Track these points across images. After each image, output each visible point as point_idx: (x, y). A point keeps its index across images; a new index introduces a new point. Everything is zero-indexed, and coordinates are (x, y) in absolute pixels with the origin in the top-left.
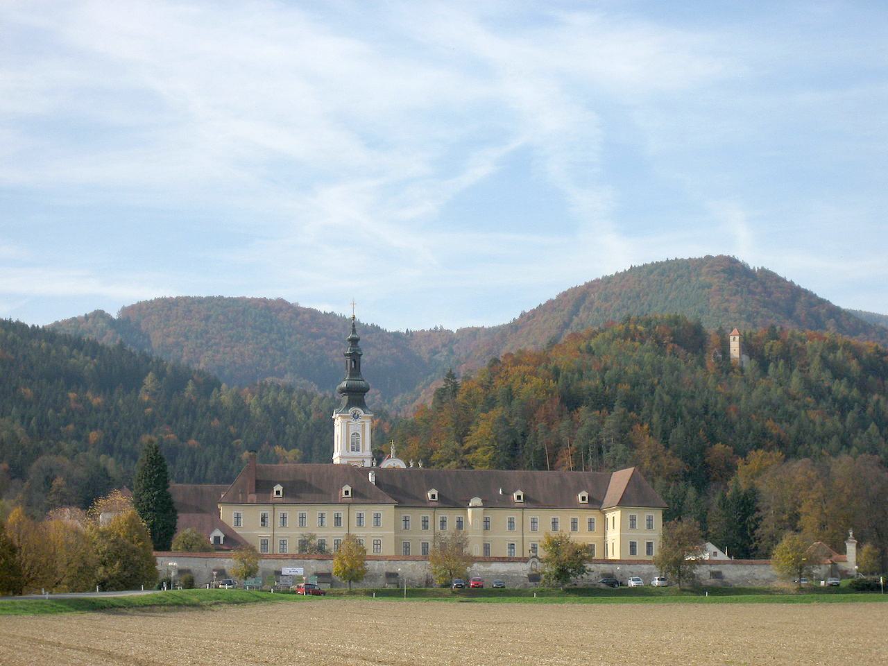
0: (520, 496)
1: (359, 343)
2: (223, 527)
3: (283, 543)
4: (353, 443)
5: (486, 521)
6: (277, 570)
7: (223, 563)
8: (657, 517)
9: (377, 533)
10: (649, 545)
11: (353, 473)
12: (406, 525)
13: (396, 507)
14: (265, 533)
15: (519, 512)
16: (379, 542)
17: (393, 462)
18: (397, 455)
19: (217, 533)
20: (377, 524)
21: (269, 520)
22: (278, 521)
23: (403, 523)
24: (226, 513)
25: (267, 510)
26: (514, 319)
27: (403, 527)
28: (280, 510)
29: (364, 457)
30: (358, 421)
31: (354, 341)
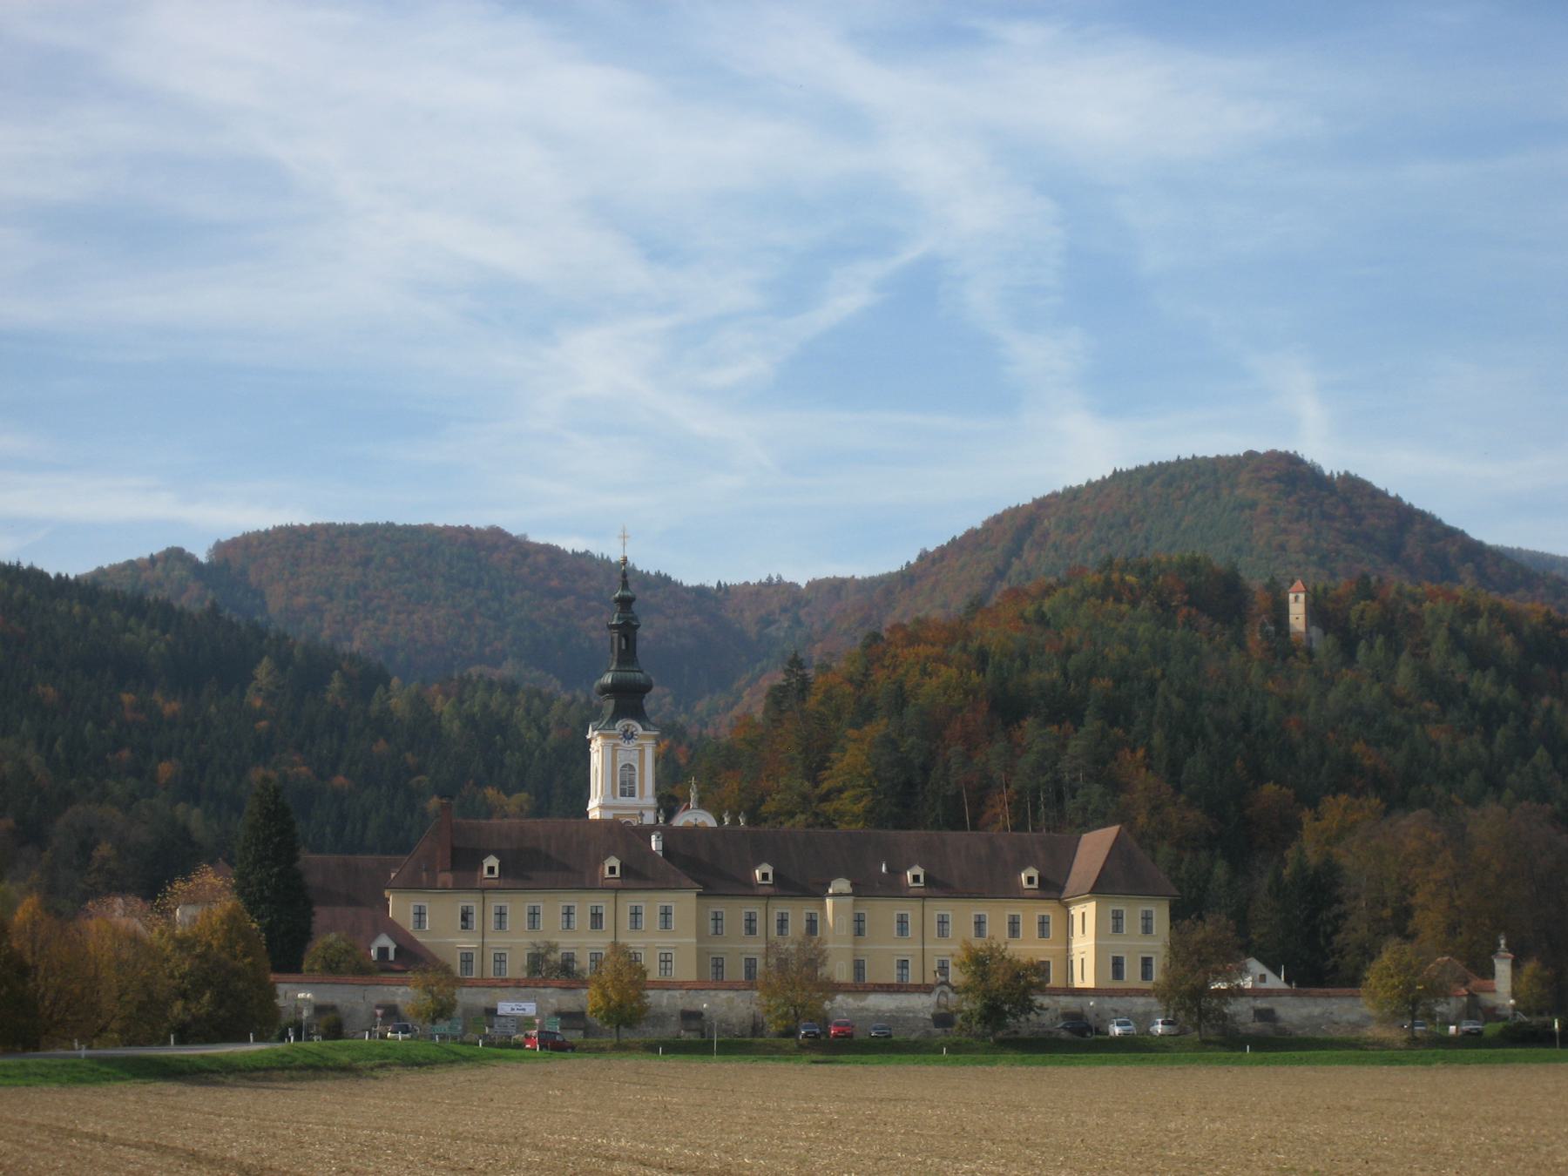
2: (394, 930)
4: (623, 783)
5: (859, 920)
8: (1161, 913)
9: (665, 941)
10: (1147, 962)
11: (624, 836)
14: (468, 942)
17: (693, 817)
18: (702, 804)
19: (384, 941)
22: (492, 918)
24: (399, 907)
30: (633, 743)
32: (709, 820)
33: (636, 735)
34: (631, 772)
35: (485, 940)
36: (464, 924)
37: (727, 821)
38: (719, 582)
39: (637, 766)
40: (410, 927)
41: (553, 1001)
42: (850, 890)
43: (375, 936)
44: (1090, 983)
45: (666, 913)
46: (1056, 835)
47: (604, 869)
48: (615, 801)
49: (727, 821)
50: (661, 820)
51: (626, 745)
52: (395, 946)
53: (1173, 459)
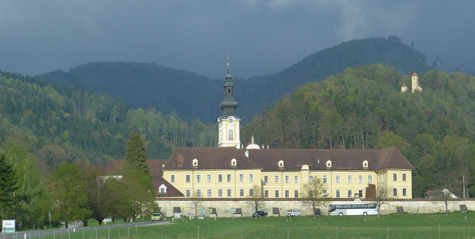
3: (287, 192)
4: (230, 136)
6: (276, 207)
7: (179, 203)
8: (409, 174)
9: (209, 186)
10: (404, 190)
11: (231, 151)
13: (262, 170)
14: (189, 186)
15: (329, 173)
16: (210, 191)
17: (253, 146)
18: (256, 142)
19: (163, 186)
20: (228, 180)
22: (196, 179)
24: (167, 175)
28: (197, 173)
29: (236, 143)
32: (257, 147)
33: (233, 121)
34: (232, 133)
35: (235, 185)
37: (263, 147)
38: (342, 41)
39: (234, 131)
41: (231, 205)
42: (308, 168)
43: (160, 185)
44: (161, 192)
45: (229, 176)
46: (372, 150)
47: (231, 163)
48: (227, 142)
49: (263, 147)
50: (242, 147)
51: (230, 124)
52: (167, 188)
53: (332, 46)
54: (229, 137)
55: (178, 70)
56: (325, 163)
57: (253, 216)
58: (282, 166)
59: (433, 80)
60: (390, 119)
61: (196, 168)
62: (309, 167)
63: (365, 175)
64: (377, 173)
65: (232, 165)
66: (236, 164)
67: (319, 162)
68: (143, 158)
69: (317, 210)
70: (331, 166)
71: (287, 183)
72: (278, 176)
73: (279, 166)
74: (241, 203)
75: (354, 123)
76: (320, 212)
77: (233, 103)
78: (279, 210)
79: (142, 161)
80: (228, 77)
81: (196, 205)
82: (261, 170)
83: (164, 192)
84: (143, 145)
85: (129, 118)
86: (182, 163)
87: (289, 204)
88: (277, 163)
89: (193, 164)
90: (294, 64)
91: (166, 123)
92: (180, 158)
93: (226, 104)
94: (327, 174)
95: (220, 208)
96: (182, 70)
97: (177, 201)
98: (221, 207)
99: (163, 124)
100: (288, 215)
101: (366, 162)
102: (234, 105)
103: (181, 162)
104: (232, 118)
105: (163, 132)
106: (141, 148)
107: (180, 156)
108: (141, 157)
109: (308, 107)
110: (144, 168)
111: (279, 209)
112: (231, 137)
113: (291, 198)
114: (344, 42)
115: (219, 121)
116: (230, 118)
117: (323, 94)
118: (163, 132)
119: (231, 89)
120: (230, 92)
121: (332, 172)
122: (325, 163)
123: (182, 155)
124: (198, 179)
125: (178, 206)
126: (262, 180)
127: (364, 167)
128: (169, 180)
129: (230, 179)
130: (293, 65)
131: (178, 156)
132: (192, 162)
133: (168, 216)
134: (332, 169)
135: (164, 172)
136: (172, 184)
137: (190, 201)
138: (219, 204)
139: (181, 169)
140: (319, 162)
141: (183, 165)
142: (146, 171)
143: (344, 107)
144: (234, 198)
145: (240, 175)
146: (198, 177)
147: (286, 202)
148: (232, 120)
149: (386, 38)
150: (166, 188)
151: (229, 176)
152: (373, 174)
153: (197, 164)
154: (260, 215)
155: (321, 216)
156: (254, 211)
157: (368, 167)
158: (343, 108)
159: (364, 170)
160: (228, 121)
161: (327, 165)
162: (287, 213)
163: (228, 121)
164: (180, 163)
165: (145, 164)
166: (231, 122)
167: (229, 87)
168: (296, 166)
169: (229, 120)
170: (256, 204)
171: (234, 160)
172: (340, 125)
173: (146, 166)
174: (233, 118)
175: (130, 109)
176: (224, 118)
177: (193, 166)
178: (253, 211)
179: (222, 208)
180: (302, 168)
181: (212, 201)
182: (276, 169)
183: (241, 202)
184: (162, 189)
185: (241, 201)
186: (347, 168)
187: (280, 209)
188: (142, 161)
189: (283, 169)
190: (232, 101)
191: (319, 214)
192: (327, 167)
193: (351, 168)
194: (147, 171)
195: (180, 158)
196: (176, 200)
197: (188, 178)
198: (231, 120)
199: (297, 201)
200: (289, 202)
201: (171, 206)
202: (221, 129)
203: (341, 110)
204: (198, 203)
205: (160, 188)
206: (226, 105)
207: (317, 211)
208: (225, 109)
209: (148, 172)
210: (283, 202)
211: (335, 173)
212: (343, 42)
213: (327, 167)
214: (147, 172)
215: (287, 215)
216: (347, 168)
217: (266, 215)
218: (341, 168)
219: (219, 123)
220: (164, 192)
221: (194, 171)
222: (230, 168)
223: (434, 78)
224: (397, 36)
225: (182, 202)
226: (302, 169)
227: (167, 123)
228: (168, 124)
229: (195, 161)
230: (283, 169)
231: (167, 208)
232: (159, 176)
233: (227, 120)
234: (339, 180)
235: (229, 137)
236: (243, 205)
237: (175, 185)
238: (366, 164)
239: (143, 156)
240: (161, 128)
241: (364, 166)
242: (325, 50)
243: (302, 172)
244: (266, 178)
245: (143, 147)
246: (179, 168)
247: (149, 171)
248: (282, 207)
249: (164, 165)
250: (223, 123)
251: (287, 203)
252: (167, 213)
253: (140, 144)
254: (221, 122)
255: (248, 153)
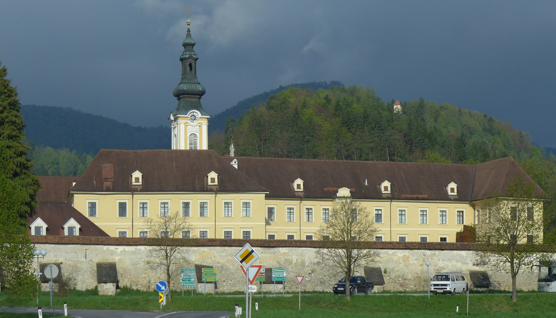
0: (387, 187)
1: (195, 48)
2: (79, 218)
4: (191, 140)
5: (271, 211)
7: (113, 253)
12: (308, 217)
19: (72, 223)
20: (202, 214)
21: (209, 211)
22: (138, 211)
23: (420, 218)
25: (125, 198)
26: (215, 115)
27: (440, 222)
28: (140, 198)
30: (196, 122)
31: (188, 46)
33: (198, 118)
36: (532, 156)
38: (280, 86)
39: (198, 135)
40: (86, 214)
42: (349, 195)
43: (66, 221)
45: (203, 206)
51: (192, 123)
52: (80, 226)
54: (190, 146)
55: (96, 116)
56: (378, 186)
57: (336, 292)
58: (300, 189)
59: (419, 111)
60: (419, 138)
61: (139, 190)
62: (351, 192)
63: (452, 209)
64: (473, 206)
65: (210, 183)
66: (216, 183)
67: (366, 184)
68: (14, 130)
69: (482, 276)
70: (390, 192)
71: (308, 221)
72: (293, 209)
73: (295, 190)
74: (282, 254)
75: (374, 138)
76: (489, 281)
77: (197, 87)
78: (383, 273)
79: (10, 137)
80: (188, 42)
81: (167, 255)
82: (264, 195)
83: (74, 235)
84: (13, 94)
85: (36, 157)
86: (111, 178)
87: (406, 259)
88: (291, 184)
89: (133, 180)
90: (227, 109)
91: (81, 164)
92: (108, 169)
93: (185, 89)
94: (384, 206)
95: (225, 268)
96: (101, 116)
97: (105, 247)
98: (228, 265)
99: (78, 165)
100: (439, 291)
101: (453, 185)
102: (199, 90)
103: (110, 177)
104: (195, 113)
105: (79, 174)
106: (9, 101)
107: (108, 165)
108: (7, 125)
109: (298, 117)
110: (15, 155)
111: (383, 270)
112: (193, 146)
113: (414, 241)
114: (283, 86)
115: (172, 118)
116: (192, 113)
117: (316, 101)
118: (79, 174)
119: (193, 64)
120: (191, 69)
121: (392, 203)
122: (378, 186)
123: (112, 164)
124: (141, 211)
125: (111, 261)
126: (265, 218)
127: (450, 195)
128: (85, 212)
129: (205, 211)
130: (226, 109)
131: (104, 165)
132: (130, 177)
133: (81, 287)
134: (392, 198)
135: (75, 195)
136: (92, 219)
137: (142, 248)
138: (223, 254)
139: (108, 190)
140: (366, 184)
141: (113, 183)
142: (20, 163)
143: (349, 119)
144: (261, 241)
145: (225, 203)
146: (141, 206)
147: (400, 253)
148: (195, 116)
149: (328, 83)
150: (78, 226)
151: (203, 206)
152: (466, 208)
153: (140, 180)
154: (356, 290)
155: (493, 292)
156: (342, 276)
157: (456, 194)
158: (348, 121)
159: (450, 200)
160: (189, 119)
161: (383, 189)
162: (435, 285)
163: (189, 119)
164: (107, 179)
165: (19, 145)
166: (194, 121)
167: (190, 60)
168: (325, 189)
169: (189, 116)
170: (349, 257)
171: (213, 175)
172: (352, 142)
173: (21, 149)
174: (198, 114)
175: (37, 147)
176: (182, 113)
177: (133, 184)
178: (313, 275)
179: (231, 267)
180: (337, 194)
181: (202, 249)
182: (290, 195)
183: (282, 252)
184: (71, 229)
185: (281, 249)
186: (420, 196)
187: (385, 272)
188: (10, 137)
189: (302, 194)
190: (194, 85)
191: (488, 285)
192: (383, 192)
193: (426, 196)
194: (24, 164)
195: (108, 169)
196: (105, 245)
197: (122, 208)
198: (193, 118)
199: (430, 249)
200: (407, 252)
201: (88, 259)
202: (176, 133)
203: (346, 123)
204: (360, 204)
205: (66, 227)
206: (185, 90)
207: (482, 277)
208: (184, 97)
209: (27, 168)
210: (391, 252)
211: (398, 205)
212: (281, 86)
213: (383, 192)
214: (24, 167)
215: (433, 289)
216: (420, 196)
217: (370, 289)
218: (409, 196)
219: (173, 123)
220: (74, 235)
221: (134, 196)
222: (206, 189)
223: (420, 108)
224: (339, 81)
225: (121, 248)
226: (338, 195)
227: (83, 163)
228: (85, 165)
229: (137, 174)
230: (302, 194)
231: (79, 265)
232: (64, 203)
233: (187, 116)
234: (403, 217)
235: (190, 146)
236: (286, 260)
237: (97, 221)
238: (452, 190)
239: (14, 123)
240: (75, 170)
241: (450, 193)
242: (261, 95)
243: (337, 200)
244: (271, 211)
245: (13, 98)
246: (104, 188)
247: (29, 164)
248: (390, 266)
249: (74, 184)
250: (180, 121)
251: (401, 255)
252: (79, 278)
253: (6, 91)
254: (176, 119)
255: (237, 163)
